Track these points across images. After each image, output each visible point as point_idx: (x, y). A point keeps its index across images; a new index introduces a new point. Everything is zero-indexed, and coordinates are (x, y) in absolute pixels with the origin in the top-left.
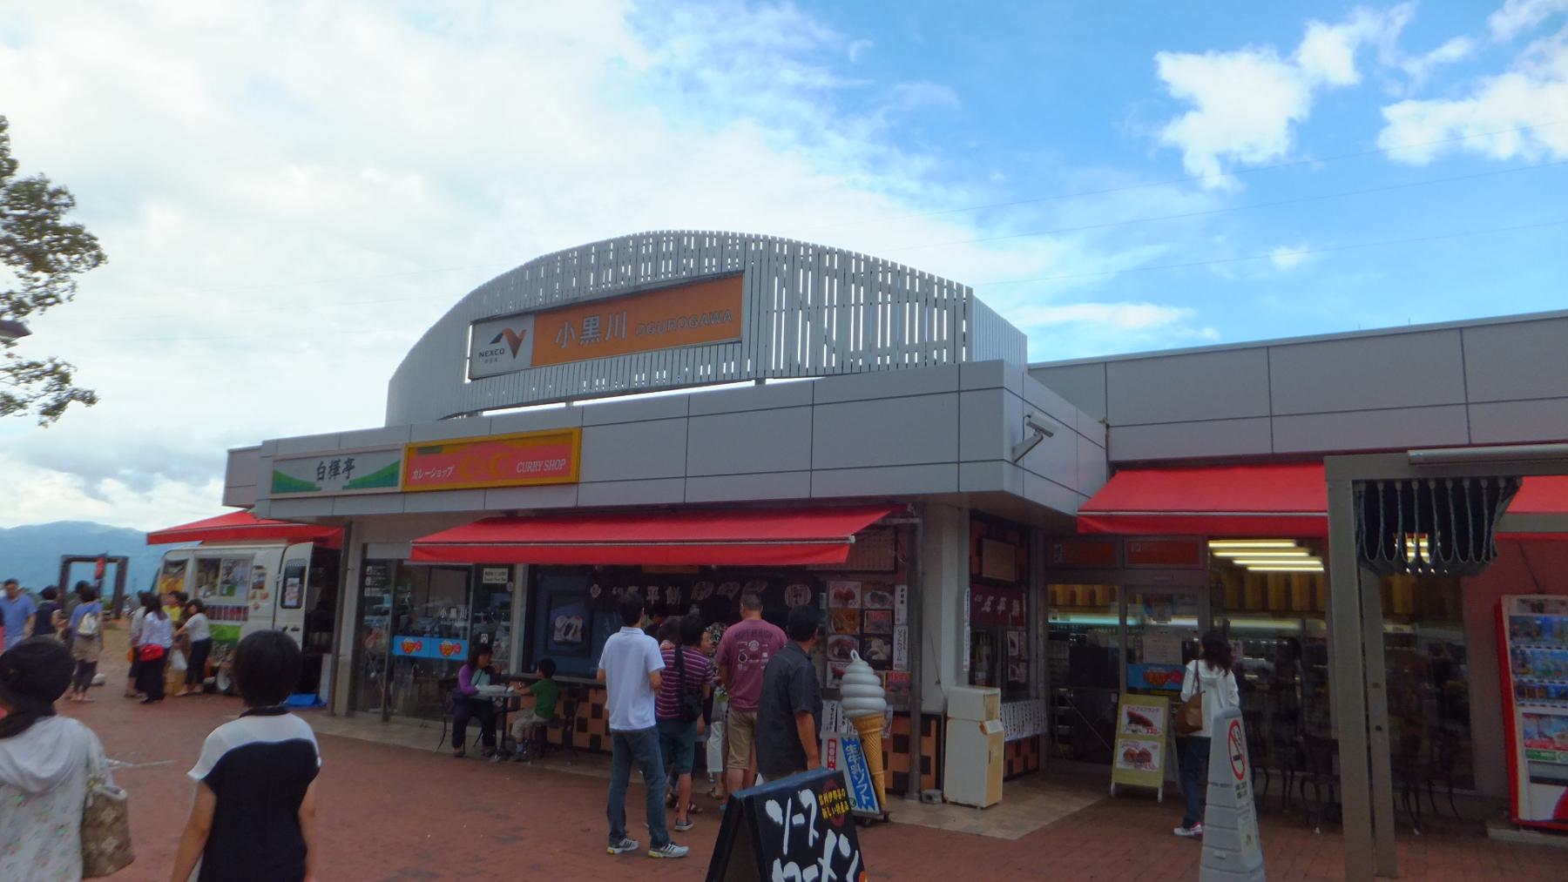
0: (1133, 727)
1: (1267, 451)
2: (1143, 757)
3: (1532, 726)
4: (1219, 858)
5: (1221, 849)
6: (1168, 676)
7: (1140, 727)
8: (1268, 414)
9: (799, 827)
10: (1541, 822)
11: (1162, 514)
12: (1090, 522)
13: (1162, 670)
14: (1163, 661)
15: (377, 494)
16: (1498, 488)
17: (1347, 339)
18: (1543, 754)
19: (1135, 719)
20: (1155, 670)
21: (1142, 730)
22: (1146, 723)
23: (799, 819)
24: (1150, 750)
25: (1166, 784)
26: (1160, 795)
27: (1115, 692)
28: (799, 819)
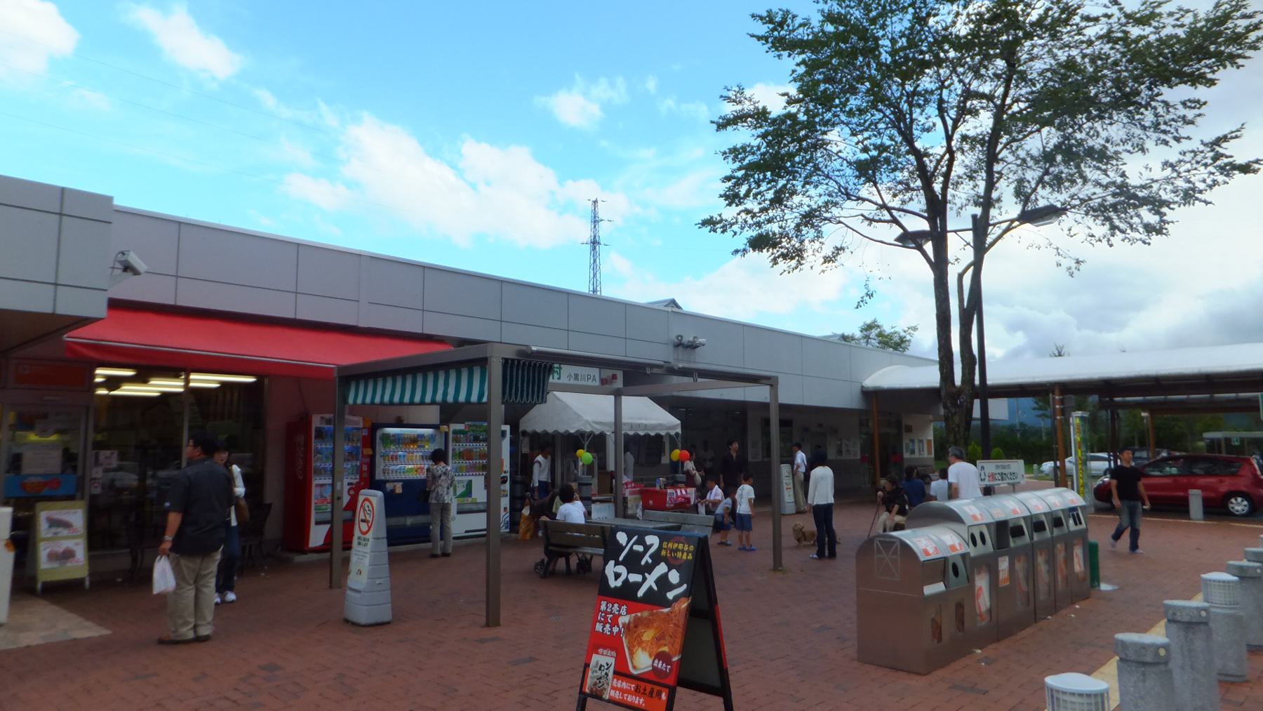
0: (54, 530)
1: (171, 302)
2: (68, 555)
3: (319, 489)
4: (379, 584)
5: (379, 578)
6: (45, 484)
7: (60, 529)
8: (298, 295)
9: (637, 552)
10: (316, 547)
11: (287, 361)
12: (84, 351)
13: (40, 479)
14: (41, 471)
15: (83, 339)
16: (508, 363)
17: (144, 216)
18: (323, 507)
19: (54, 523)
20: (33, 479)
21: (65, 532)
22: (67, 525)
23: (640, 548)
24: (74, 548)
25: (91, 575)
26: (87, 583)
27: (385, 484)
28: (640, 548)
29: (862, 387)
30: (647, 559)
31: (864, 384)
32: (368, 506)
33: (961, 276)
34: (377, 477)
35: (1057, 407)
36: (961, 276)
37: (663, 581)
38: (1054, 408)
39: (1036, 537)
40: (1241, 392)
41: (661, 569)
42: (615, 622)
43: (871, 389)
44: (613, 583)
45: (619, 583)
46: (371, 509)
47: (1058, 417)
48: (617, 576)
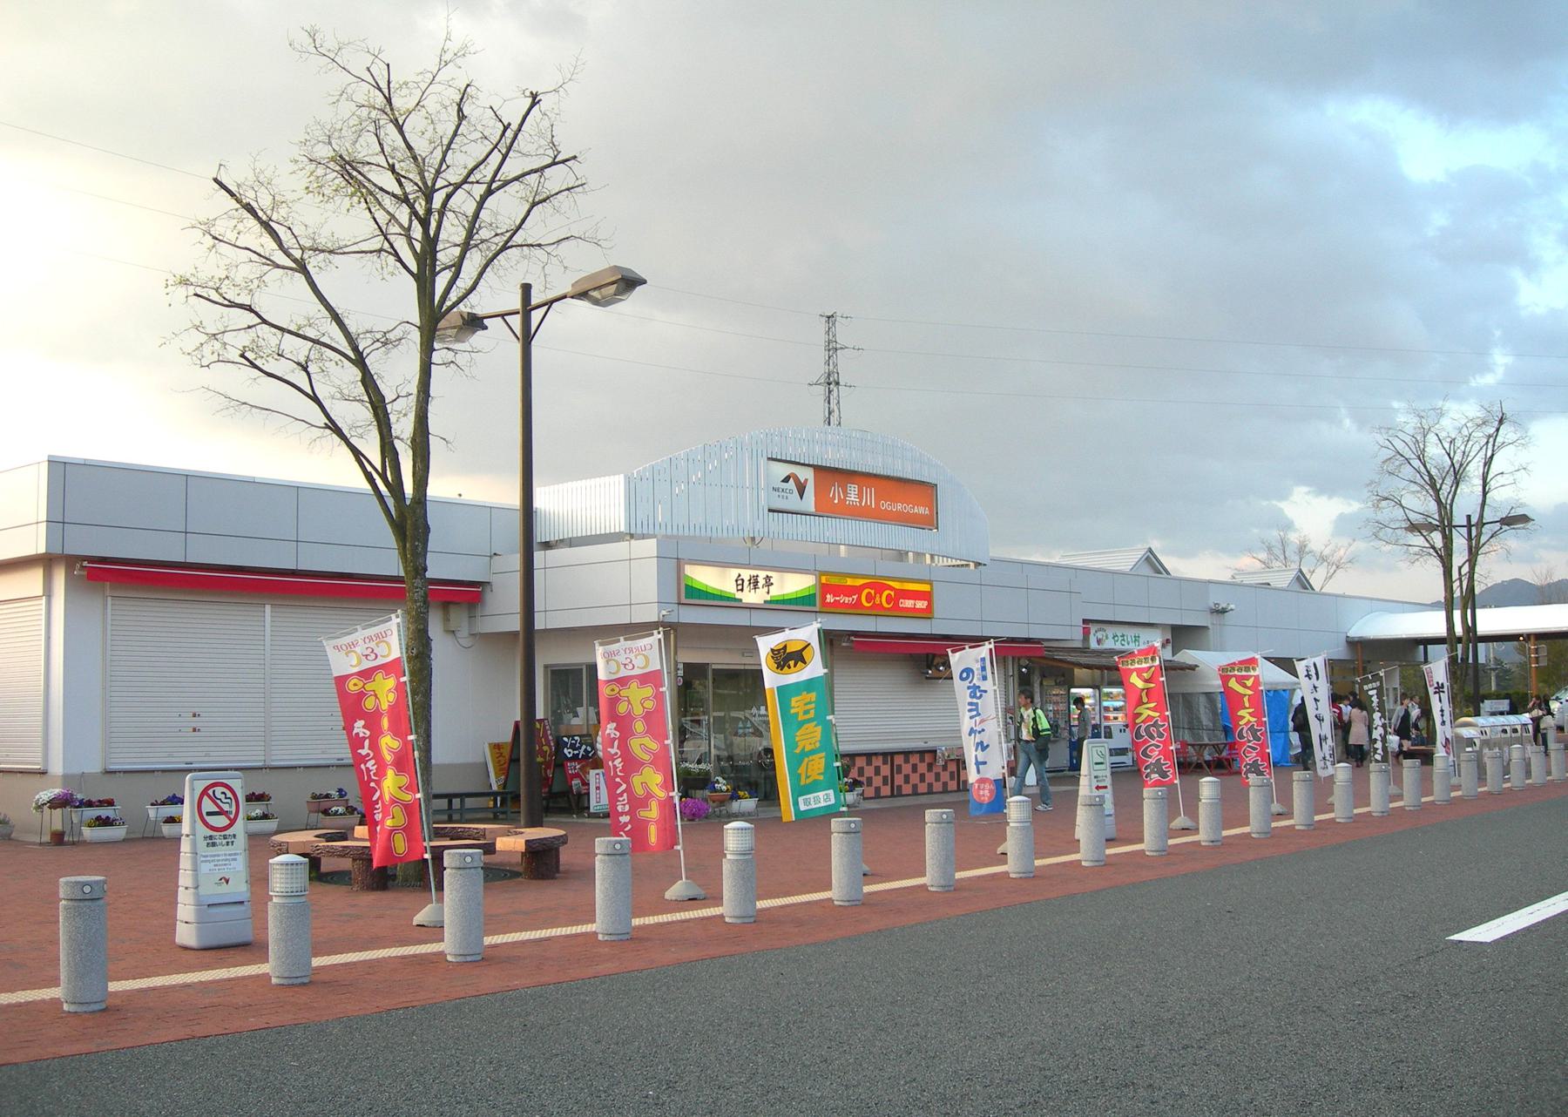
23: (573, 742)
28: (573, 742)
29: (1347, 637)
30: (578, 745)
31: (1348, 635)
32: (223, 793)
33: (1460, 568)
34: (832, 791)
35: (1532, 655)
36: (1460, 568)
37: (585, 750)
38: (1530, 657)
39: (1513, 735)
40: (389, 722)
41: (584, 747)
42: (575, 769)
43: (1356, 639)
44: (569, 756)
45: (571, 755)
46: (229, 794)
47: (1533, 666)
48: (570, 753)
